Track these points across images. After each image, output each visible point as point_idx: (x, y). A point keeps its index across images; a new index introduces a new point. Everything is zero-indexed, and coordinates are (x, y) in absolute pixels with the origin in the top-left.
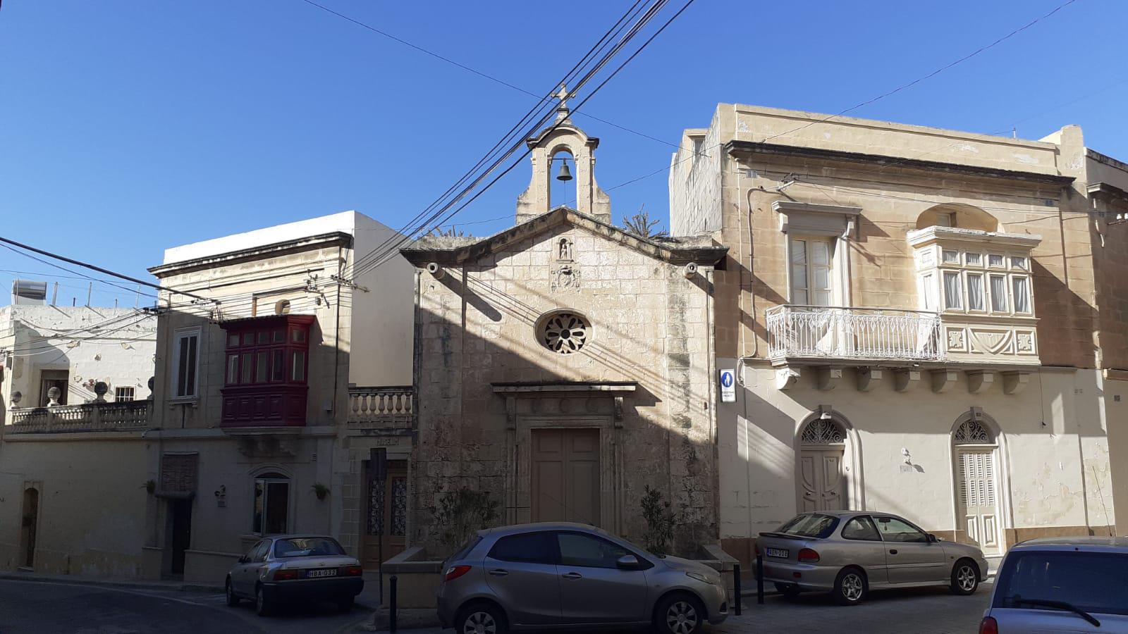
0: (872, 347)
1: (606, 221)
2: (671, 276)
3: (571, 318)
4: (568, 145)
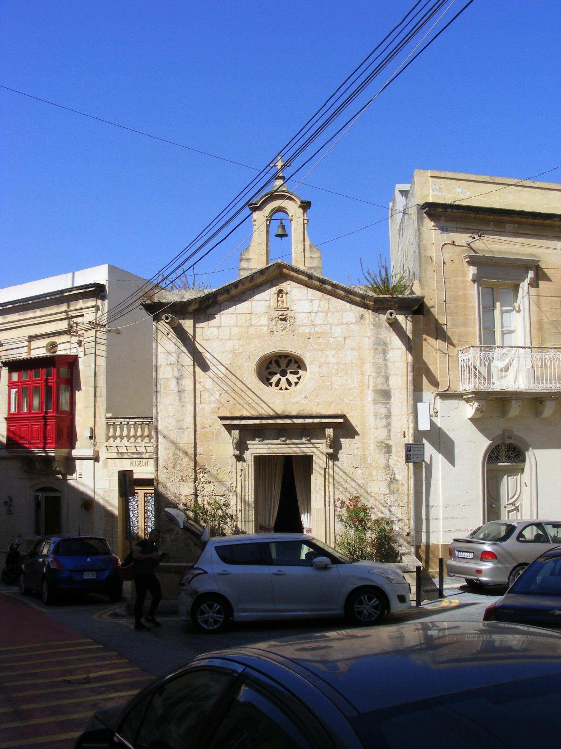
0: (547, 380)
1: (316, 274)
3: (288, 359)
4: (285, 208)
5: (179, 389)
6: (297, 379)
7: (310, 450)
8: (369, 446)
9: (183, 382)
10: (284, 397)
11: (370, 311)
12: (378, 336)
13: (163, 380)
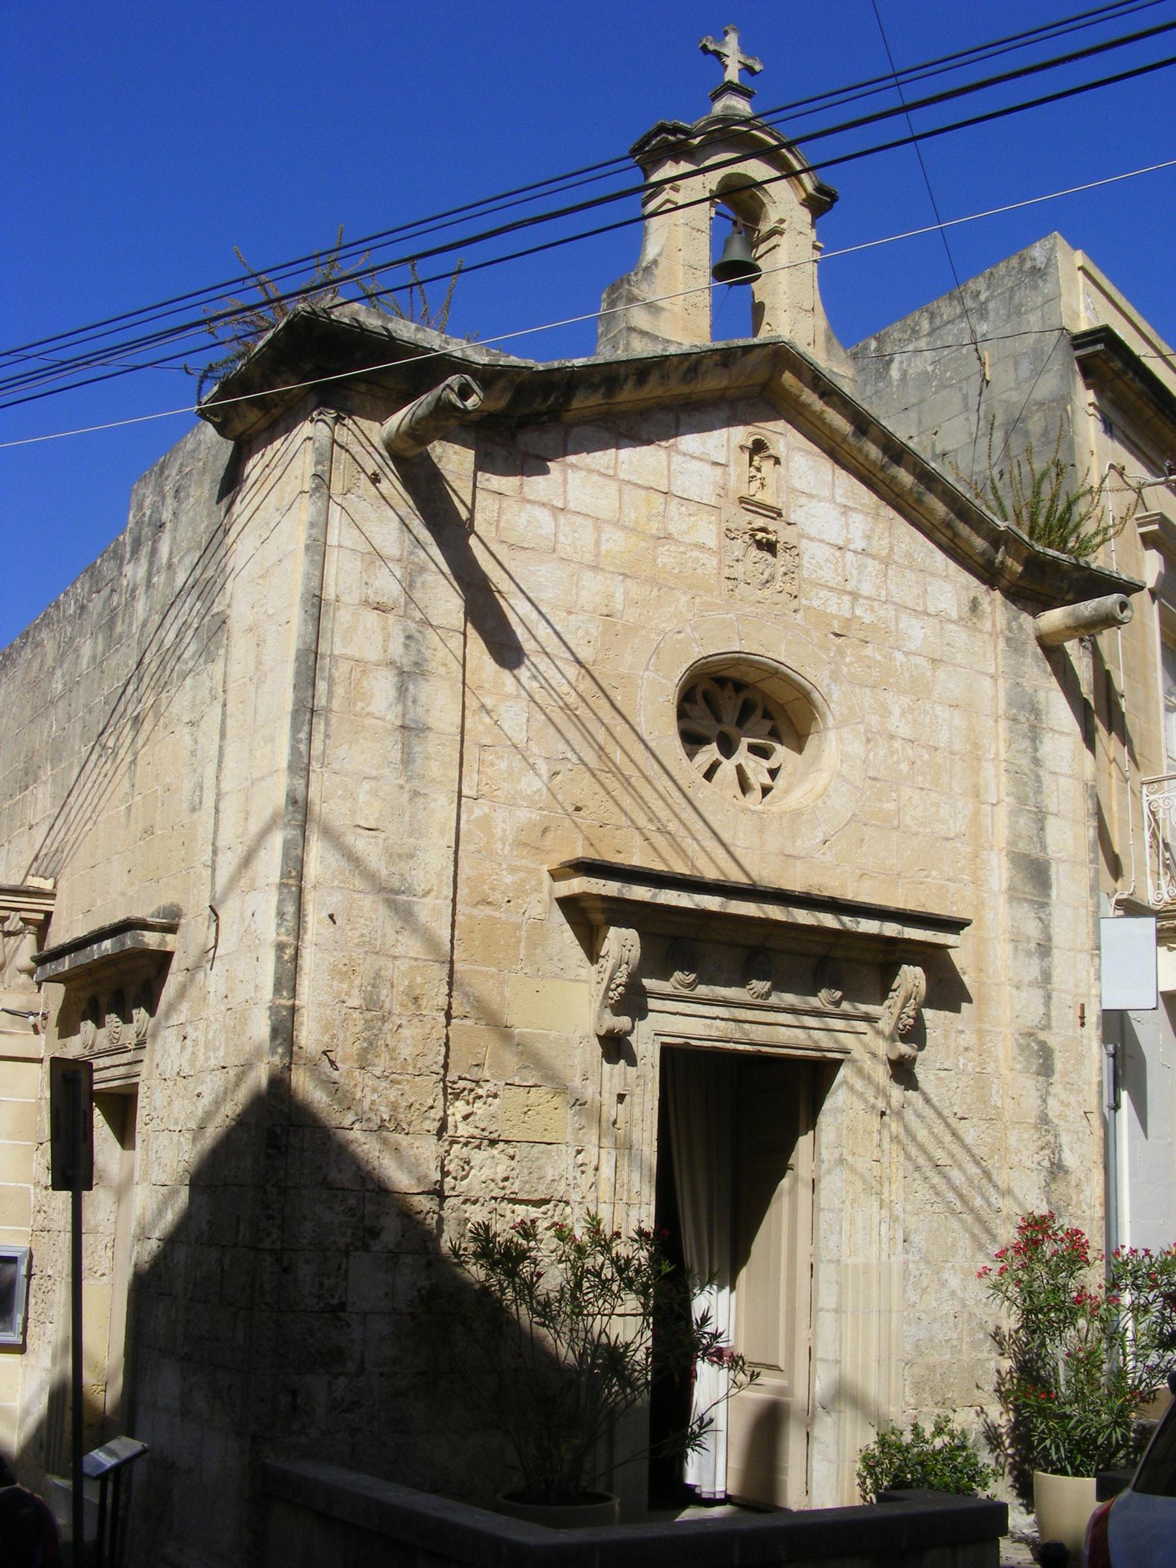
2: (1010, 630)
5: (404, 715)
6: (767, 775)
7: (837, 1041)
8: (995, 1045)
9: (424, 690)
10: (762, 831)
11: (997, 594)
12: (1020, 680)
13: (344, 667)
